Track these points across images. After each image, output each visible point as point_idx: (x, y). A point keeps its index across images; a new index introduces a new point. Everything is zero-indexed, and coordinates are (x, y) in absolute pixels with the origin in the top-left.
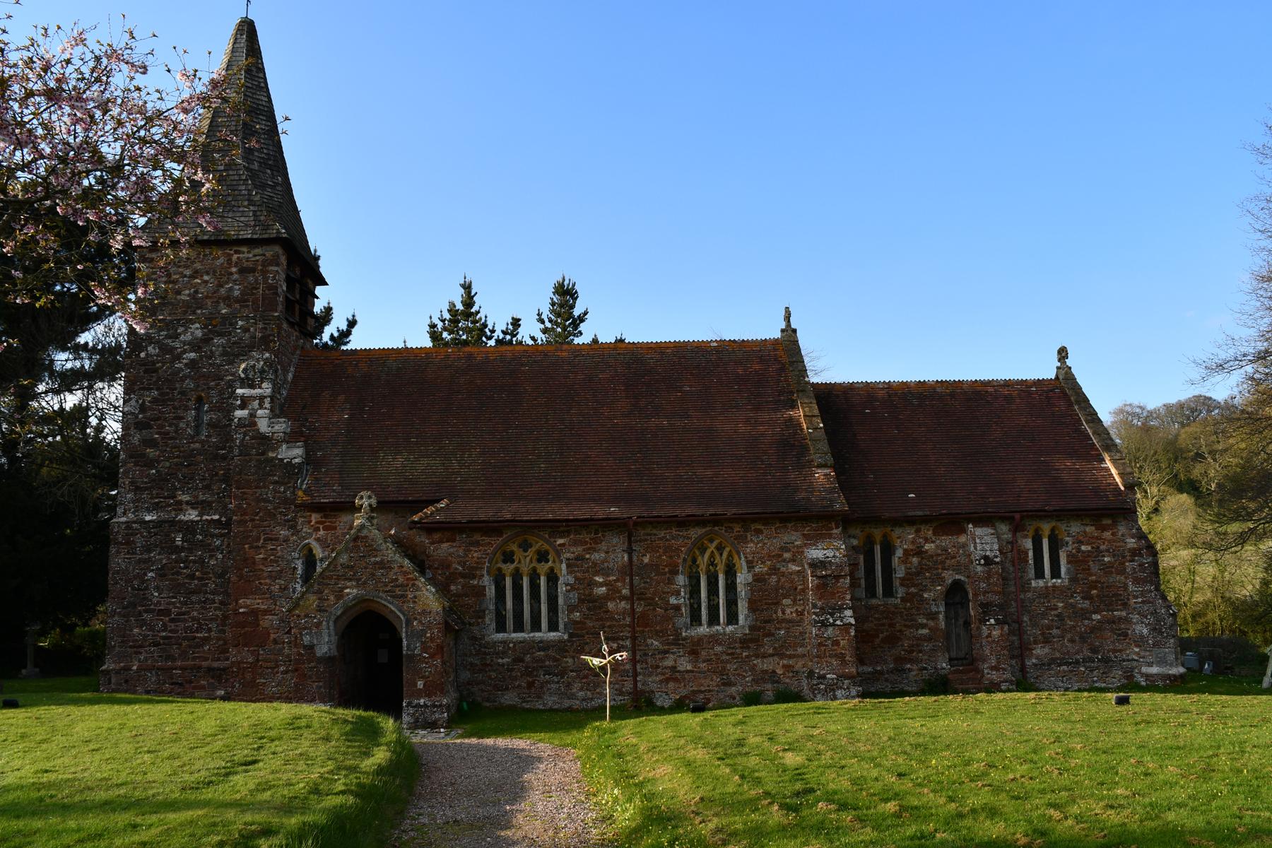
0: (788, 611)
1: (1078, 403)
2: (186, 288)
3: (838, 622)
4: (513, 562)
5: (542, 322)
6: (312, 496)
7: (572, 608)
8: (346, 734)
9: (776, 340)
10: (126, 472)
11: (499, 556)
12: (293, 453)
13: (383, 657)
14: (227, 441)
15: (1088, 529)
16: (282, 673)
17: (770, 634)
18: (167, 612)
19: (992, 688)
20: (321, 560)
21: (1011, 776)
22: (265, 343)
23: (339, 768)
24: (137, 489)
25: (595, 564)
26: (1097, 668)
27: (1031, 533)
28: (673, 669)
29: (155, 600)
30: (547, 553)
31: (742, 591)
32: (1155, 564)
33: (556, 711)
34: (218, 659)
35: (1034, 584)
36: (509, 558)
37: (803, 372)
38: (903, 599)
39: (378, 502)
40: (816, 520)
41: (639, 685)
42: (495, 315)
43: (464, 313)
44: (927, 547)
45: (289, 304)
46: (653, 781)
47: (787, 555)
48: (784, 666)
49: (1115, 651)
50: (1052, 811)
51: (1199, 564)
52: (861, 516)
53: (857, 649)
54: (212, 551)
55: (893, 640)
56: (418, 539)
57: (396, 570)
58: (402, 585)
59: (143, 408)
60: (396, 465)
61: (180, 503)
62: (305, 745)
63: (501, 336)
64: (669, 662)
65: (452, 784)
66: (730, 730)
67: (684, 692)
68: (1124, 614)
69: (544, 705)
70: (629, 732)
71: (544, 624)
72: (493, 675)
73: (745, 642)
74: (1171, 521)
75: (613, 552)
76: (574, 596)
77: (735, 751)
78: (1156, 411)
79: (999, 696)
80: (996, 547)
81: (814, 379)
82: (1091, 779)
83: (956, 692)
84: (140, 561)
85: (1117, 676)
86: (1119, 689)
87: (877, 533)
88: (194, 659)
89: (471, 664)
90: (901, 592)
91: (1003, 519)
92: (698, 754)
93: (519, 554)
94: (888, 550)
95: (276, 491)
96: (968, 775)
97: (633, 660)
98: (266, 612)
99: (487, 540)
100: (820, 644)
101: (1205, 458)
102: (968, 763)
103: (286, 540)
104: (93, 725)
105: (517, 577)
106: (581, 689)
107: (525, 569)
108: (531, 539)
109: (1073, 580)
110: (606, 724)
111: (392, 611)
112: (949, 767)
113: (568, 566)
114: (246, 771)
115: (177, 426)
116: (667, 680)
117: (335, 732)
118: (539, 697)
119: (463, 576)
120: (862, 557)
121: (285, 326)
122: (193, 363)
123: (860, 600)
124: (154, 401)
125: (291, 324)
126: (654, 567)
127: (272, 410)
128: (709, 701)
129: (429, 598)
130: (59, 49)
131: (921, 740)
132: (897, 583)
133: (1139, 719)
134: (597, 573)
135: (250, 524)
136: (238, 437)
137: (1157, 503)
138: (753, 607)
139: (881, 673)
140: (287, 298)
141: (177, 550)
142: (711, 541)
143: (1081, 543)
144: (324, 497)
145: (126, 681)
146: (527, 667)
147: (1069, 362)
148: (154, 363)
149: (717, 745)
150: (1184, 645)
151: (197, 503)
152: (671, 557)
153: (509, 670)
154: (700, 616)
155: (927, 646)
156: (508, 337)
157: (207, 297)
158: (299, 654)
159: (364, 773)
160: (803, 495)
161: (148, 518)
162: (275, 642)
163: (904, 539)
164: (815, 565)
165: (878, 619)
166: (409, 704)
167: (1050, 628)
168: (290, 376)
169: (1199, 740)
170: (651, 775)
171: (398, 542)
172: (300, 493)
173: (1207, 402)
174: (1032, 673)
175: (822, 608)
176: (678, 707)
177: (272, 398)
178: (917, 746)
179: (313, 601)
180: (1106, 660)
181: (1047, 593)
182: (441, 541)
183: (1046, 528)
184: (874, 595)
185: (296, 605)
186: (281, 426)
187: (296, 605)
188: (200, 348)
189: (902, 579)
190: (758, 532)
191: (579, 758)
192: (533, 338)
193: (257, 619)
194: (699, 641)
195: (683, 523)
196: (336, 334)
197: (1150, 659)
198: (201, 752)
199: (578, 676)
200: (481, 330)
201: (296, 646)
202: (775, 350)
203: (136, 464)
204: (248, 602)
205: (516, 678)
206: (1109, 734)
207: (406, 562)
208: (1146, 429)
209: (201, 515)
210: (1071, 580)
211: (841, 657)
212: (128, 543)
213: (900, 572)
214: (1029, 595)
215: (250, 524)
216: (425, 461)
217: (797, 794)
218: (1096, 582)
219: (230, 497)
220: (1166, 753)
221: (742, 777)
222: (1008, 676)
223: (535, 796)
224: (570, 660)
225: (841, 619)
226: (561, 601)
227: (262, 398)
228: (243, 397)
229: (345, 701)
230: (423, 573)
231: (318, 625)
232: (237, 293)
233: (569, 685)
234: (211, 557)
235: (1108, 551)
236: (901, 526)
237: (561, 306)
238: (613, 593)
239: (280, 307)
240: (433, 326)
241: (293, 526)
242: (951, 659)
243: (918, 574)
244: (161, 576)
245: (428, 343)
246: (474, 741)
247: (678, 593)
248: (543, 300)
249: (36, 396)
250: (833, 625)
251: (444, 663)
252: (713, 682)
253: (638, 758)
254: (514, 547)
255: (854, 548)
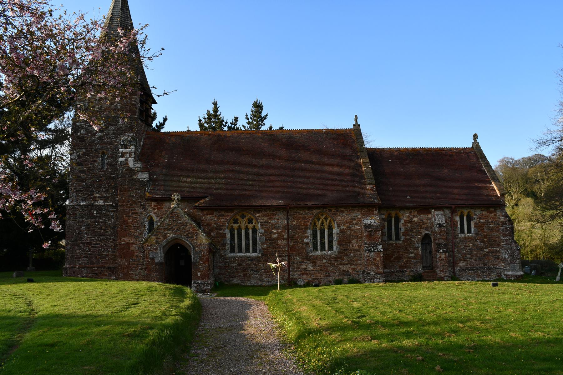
0: (354, 245)
1: (481, 158)
2: (97, 105)
3: (376, 251)
4: (238, 223)
5: (248, 119)
6: (152, 194)
7: (262, 243)
8: (172, 293)
9: (351, 129)
10: (72, 184)
11: (232, 221)
12: (144, 177)
13: (182, 263)
14: (115, 171)
15: (484, 213)
16: (140, 269)
17: (346, 255)
18: (90, 244)
19: (441, 279)
20: (156, 222)
21: (445, 312)
22: (130, 129)
23: (172, 306)
24: (77, 191)
25: (273, 225)
26: (486, 272)
27: (459, 214)
28: (305, 269)
29: (85, 238)
30: (252, 219)
31: (335, 237)
32: (512, 228)
33: (256, 286)
34: (112, 264)
35: (460, 235)
36: (236, 222)
37: (362, 143)
38: (403, 241)
39: (181, 198)
40: (367, 207)
41: (291, 276)
42: (227, 116)
43: (214, 116)
44: (414, 219)
45: (141, 112)
46: (300, 312)
47: (354, 222)
48: (352, 269)
49: (493, 265)
50: (459, 324)
51: (532, 228)
52: (387, 205)
53: (384, 262)
54: (109, 218)
55: (399, 258)
56: (197, 213)
57: (189, 226)
58: (191, 233)
59: (79, 157)
60: (187, 181)
61: (95, 197)
62: (156, 298)
63: (230, 125)
64: (304, 266)
65: (216, 314)
66: (331, 294)
67: (310, 279)
68: (498, 249)
69: (251, 284)
70: (288, 294)
71: (251, 250)
72: (229, 271)
73: (336, 258)
74: (522, 211)
75: (280, 220)
76: (264, 238)
77: (333, 301)
78: (519, 161)
79: (443, 282)
80: (444, 219)
81: (367, 146)
82: (477, 313)
83: (425, 281)
84: (79, 222)
85: (494, 275)
86: (495, 281)
87: (393, 213)
88: (102, 263)
89: (220, 266)
90: (403, 238)
91: (447, 208)
92: (318, 302)
93: (240, 220)
94: (398, 220)
95: (137, 193)
96: (427, 311)
97: (288, 265)
98: (133, 244)
99: (227, 214)
100: (368, 260)
101: (539, 182)
102: (428, 307)
103: (141, 213)
104: (68, 289)
105: (239, 229)
106: (266, 277)
107: (243, 226)
108: (245, 214)
109: (477, 234)
110: (278, 291)
111: (187, 244)
112: (420, 308)
113: (261, 225)
114: (135, 307)
115: (94, 164)
116: (303, 274)
117: (167, 293)
118: (249, 281)
119: (216, 229)
120: (386, 223)
121: (139, 121)
122: (100, 138)
123: (385, 241)
124: (84, 153)
125: (142, 121)
126: (298, 226)
127: (135, 158)
128: (320, 283)
129: (203, 238)
130: (74, 21)
131: (409, 298)
132: (401, 234)
133: (500, 292)
134: (273, 228)
135: (126, 207)
136: (120, 170)
137: (517, 201)
138: (340, 244)
139: (394, 272)
140: (140, 109)
141: (95, 217)
142: (322, 215)
143: (480, 218)
144: (157, 195)
145: (74, 272)
146: (244, 268)
147: (478, 140)
148: (83, 137)
149: (325, 299)
150: (524, 264)
151: (103, 197)
152: (305, 222)
153: (236, 269)
154: (317, 247)
155: (413, 261)
156: (233, 126)
157: (106, 109)
158: (148, 261)
159: (182, 308)
160: (362, 196)
161: (82, 204)
162: (137, 256)
163: (405, 216)
164: (367, 226)
165: (393, 250)
166: (194, 283)
167: (466, 254)
168: (142, 143)
169: (523, 300)
170: (299, 310)
171: (189, 215)
172: (147, 194)
173: (540, 157)
174: (458, 273)
175: (369, 245)
176: (308, 285)
177: (135, 152)
178: (408, 301)
179: (153, 239)
180: (489, 269)
181: (465, 240)
182: (207, 214)
183: (466, 212)
184: (391, 239)
185: (147, 241)
186: (139, 165)
187: (147, 241)
188: (103, 131)
189: (403, 233)
190: (342, 212)
191: (267, 305)
192: (244, 126)
193: (129, 247)
194: (317, 257)
195: (310, 208)
196: (158, 124)
197: (508, 268)
198: (114, 300)
199: (265, 272)
200: (221, 123)
201: (147, 258)
202: (350, 133)
203: (77, 181)
204: (125, 239)
205: (238, 272)
206: (486, 297)
207: (193, 223)
208: (514, 169)
209: (104, 202)
210: (476, 234)
211: (377, 265)
212: (74, 214)
213: (403, 230)
214: (458, 240)
215: (126, 207)
216: (200, 180)
217: (359, 317)
218: (487, 235)
219: (117, 195)
220: (509, 304)
221: (336, 311)
222: (447, 274)
223: (251, 318)
224: (262, 265)
225: (377, 249)
226: (258, 240)
227: (130, 153)
228: (122, 152)
229: (167, 280)
230: (200, 228)
231: (156, 249)
232: (119, 107)
233: (261, 275)
234: (109, 220)
235: (492, 222)
236: (403, 210)
237: (256, 112)
238: (280, 237)
239: (137, 114)
240: (200, 121)
241: (144, 208)
242: (423, 267)
243: (410, 230)
244: (88, 228)
245: (198, 129)
246: (223, 298)
247: (308, 237)
248: (248, 110)
249: (31, 151)
250: (374, 251)
251: (209, 265)
252: (322, 275)
253: (293, 304)
254: (238, 217)
255: (383, 219)
